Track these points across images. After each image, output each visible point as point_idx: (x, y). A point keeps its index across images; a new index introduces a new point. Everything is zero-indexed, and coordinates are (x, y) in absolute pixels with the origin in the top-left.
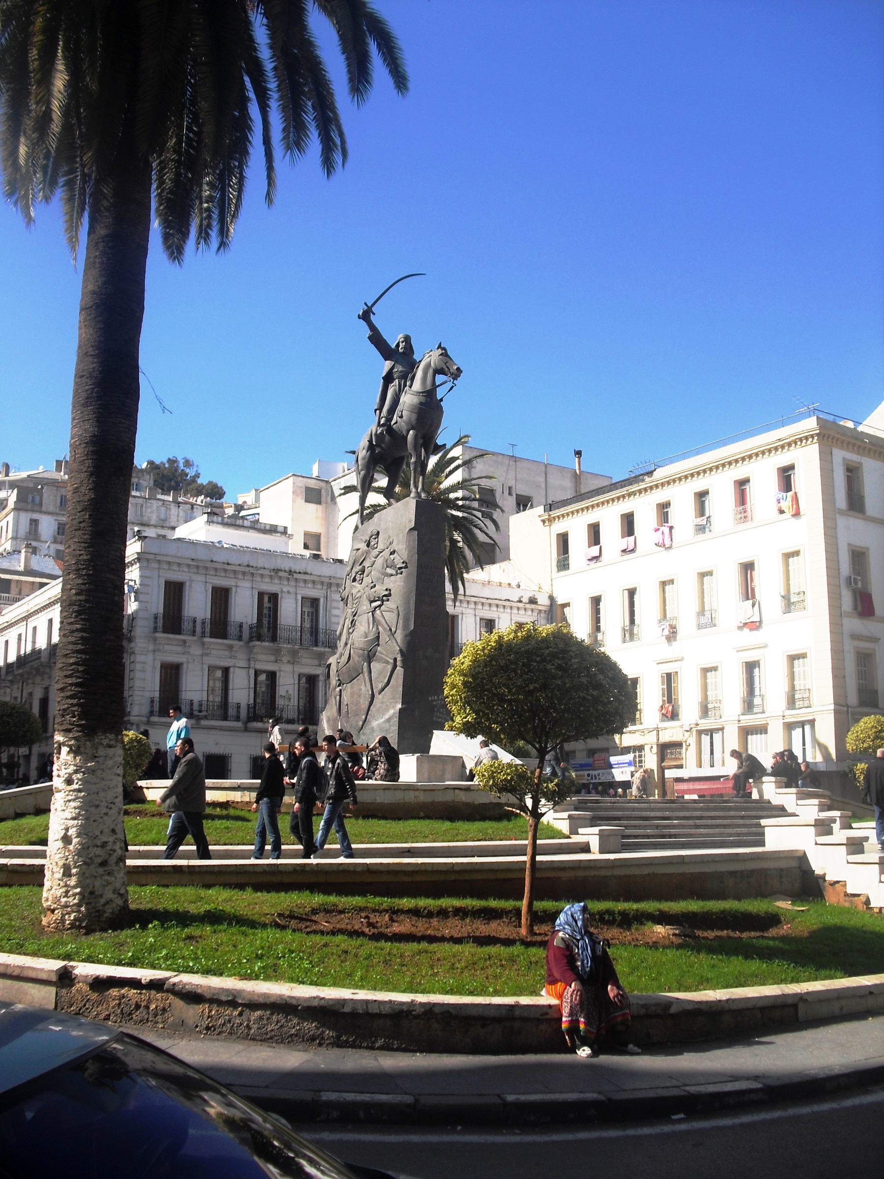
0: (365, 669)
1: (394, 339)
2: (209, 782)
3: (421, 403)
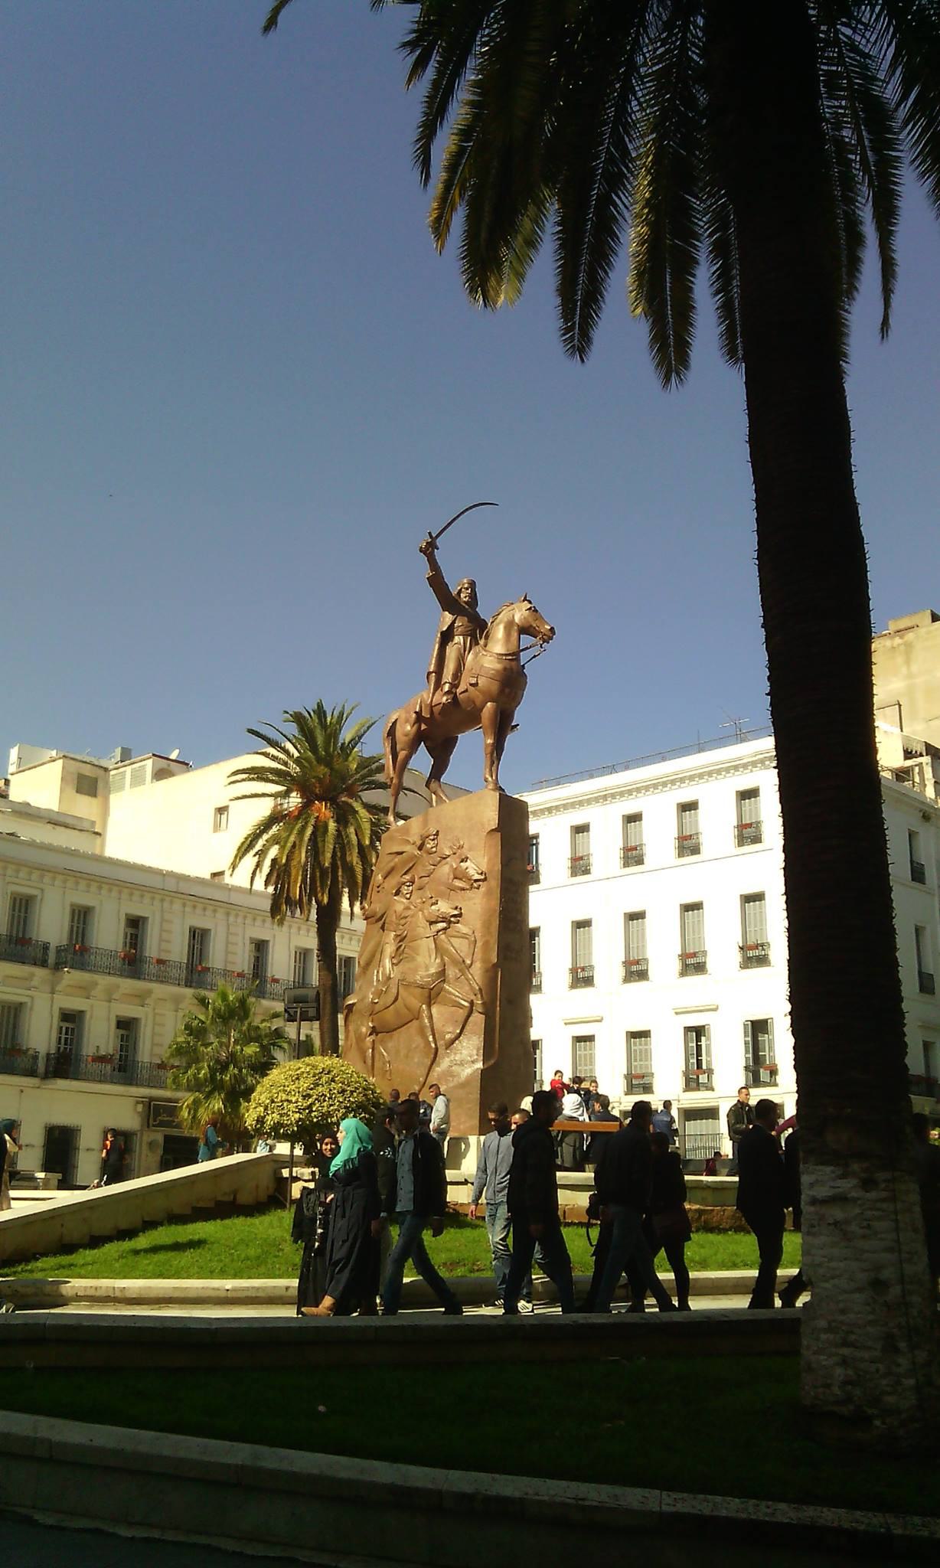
0: (425, 1014)
1: (456, 584)
2: (13, 1193)
3: (505, 669)
